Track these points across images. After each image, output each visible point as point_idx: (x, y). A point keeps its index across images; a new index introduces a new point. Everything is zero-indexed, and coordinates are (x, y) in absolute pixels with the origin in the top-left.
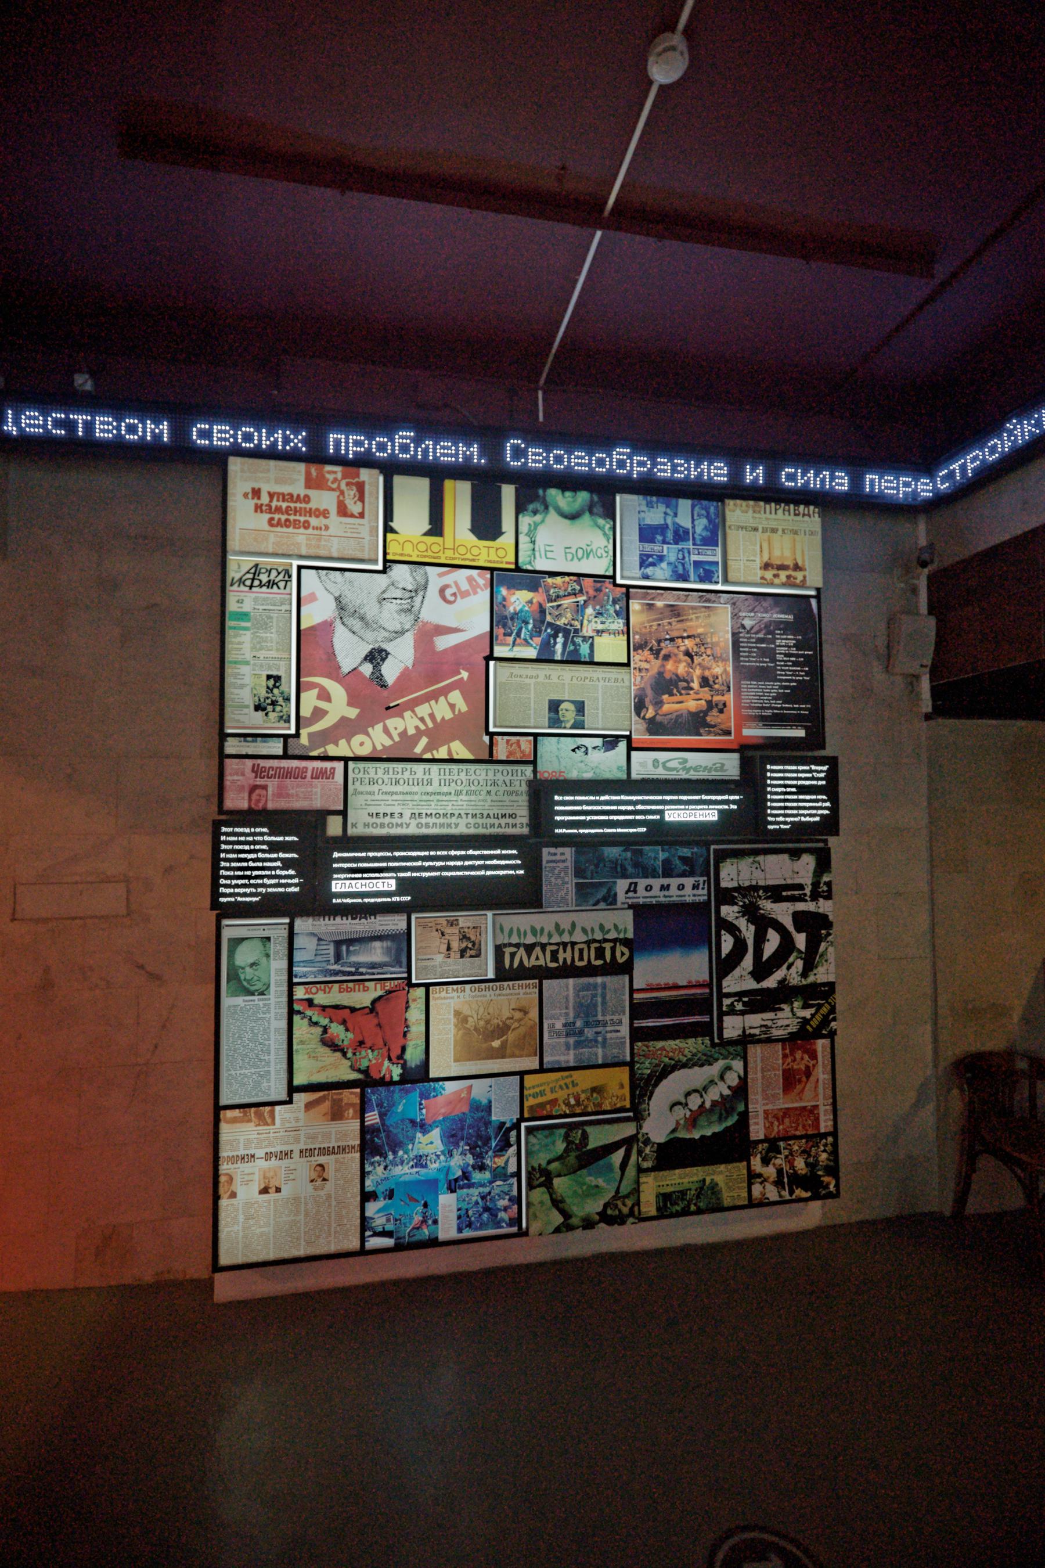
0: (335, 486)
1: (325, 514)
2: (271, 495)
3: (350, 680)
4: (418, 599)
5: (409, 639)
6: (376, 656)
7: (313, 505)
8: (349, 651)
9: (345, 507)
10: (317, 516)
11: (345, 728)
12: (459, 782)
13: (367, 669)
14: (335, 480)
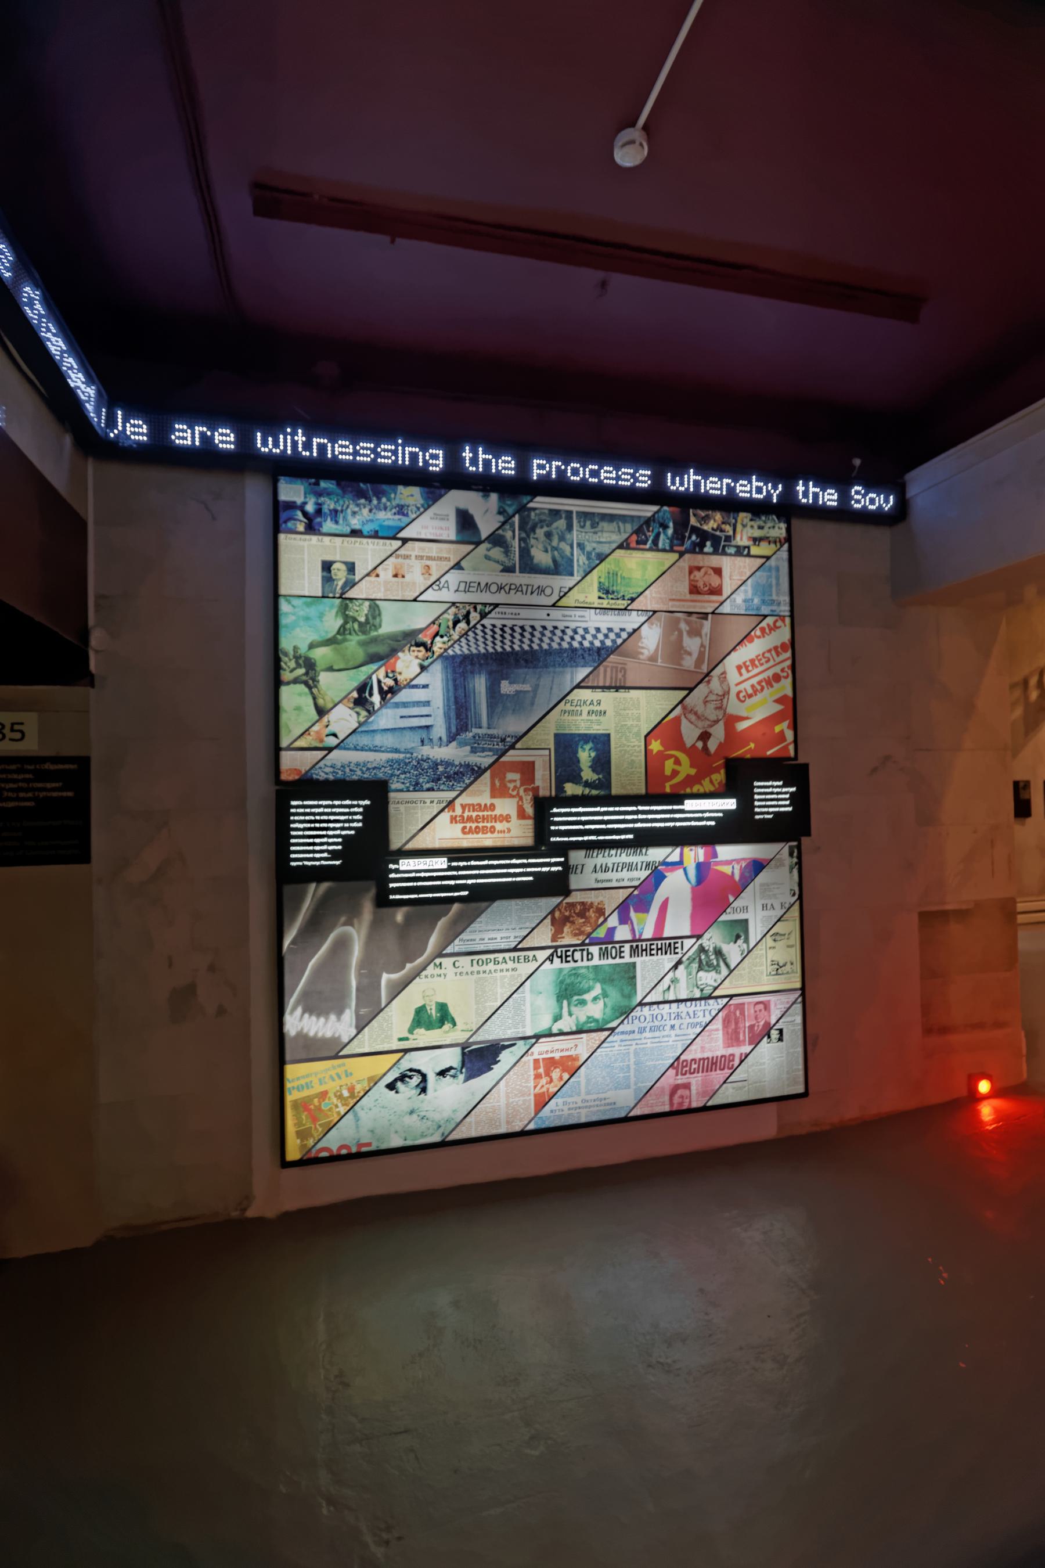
0: (514, 793)
1: (507, 818)
2: (463, 807)
3: (691, 752)
4: (725, 701)
5: (721, 724)
6: (705, 736)
7: (497, 812)
8: (690, 733)
9: (524, 810)
10: (501, 822)
11: (689, 780)
12: (642, 1019)
13: (700, 745)
14: (515, 788)
